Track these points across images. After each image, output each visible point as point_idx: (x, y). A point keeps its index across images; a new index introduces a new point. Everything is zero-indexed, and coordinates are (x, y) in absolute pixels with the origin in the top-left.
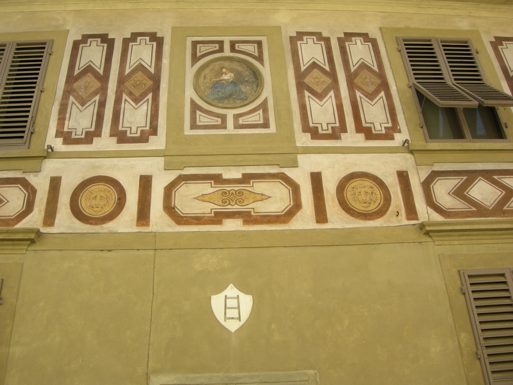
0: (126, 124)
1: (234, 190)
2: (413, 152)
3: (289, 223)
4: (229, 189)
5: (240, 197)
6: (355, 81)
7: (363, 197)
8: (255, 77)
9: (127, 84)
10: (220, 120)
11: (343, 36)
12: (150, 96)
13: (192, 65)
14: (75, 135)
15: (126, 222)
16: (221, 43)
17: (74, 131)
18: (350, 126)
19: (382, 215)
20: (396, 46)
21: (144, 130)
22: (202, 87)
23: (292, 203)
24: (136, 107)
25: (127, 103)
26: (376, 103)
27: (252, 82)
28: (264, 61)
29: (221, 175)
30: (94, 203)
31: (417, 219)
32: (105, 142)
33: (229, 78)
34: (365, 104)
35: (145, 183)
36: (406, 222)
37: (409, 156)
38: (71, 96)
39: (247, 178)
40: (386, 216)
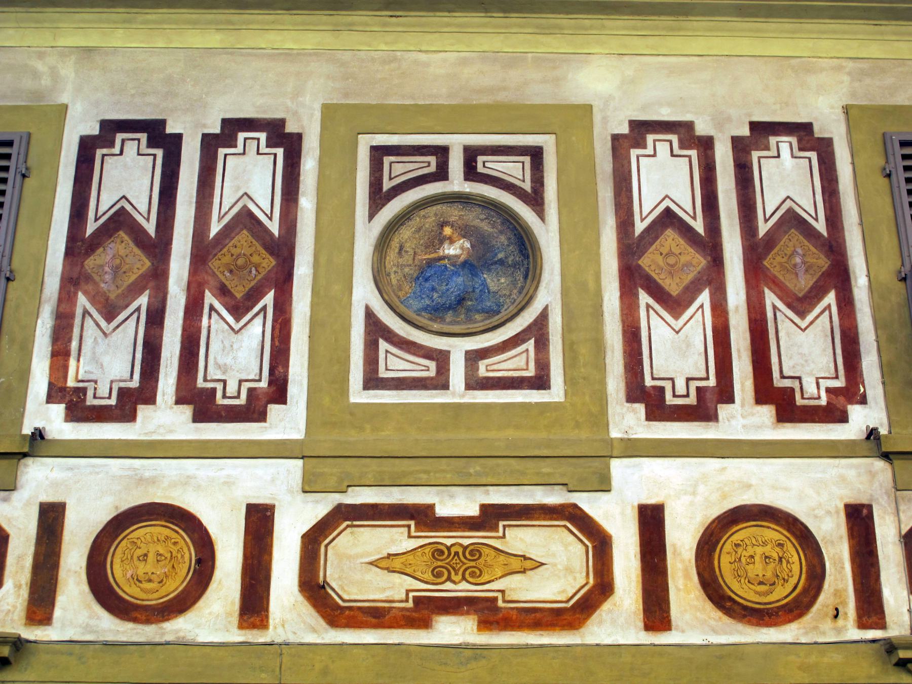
0: (214, 373)
1: (461, 545)
2: (891, 456)
3: (582, 630)
4: (449, 542)
5: (473, 564)
6: (765, 263)
7: (757, 569)
8: (521, 251)
9: (214, 264)
10: (432, 365)
11: (745, 132)
12: (269, 299)
13: (371, 216)
14: (95, 397)
15: (212, 619)
16: (442, 152)
17: (90, 386)
18: (743, 385)
19: (800, 615)
20: (882, 162)
21: (254, 389)
22: (393, 276)
23: (591, 581)
24: (237, 327)
25: (214, 314)
26: (811, 323)
27: (515, 265)
28: (546, 206)
29: (431, 507)
30: (142, 569)
31: (883, 626)
32: (165, 418)
33: (458, 252)
34: (785, 327)
35: (259, 522)
36: (855, 634)
37: (880, 464)
38: (80, 294)
39: (491, 517)
40: (808, 618)
